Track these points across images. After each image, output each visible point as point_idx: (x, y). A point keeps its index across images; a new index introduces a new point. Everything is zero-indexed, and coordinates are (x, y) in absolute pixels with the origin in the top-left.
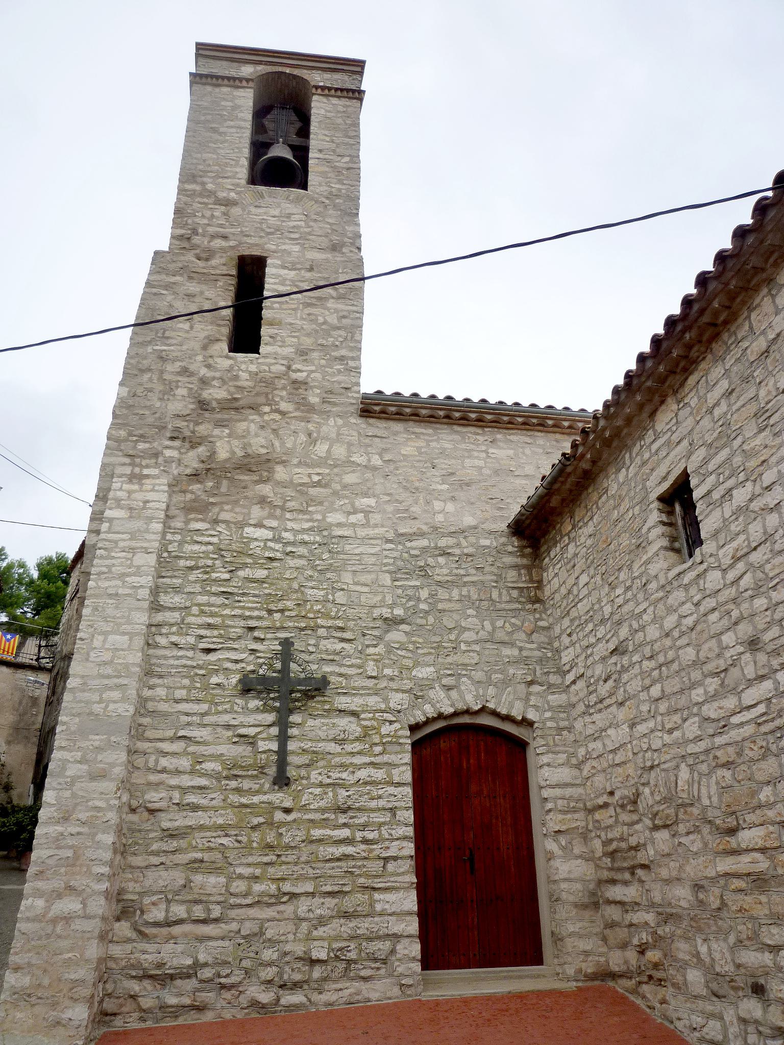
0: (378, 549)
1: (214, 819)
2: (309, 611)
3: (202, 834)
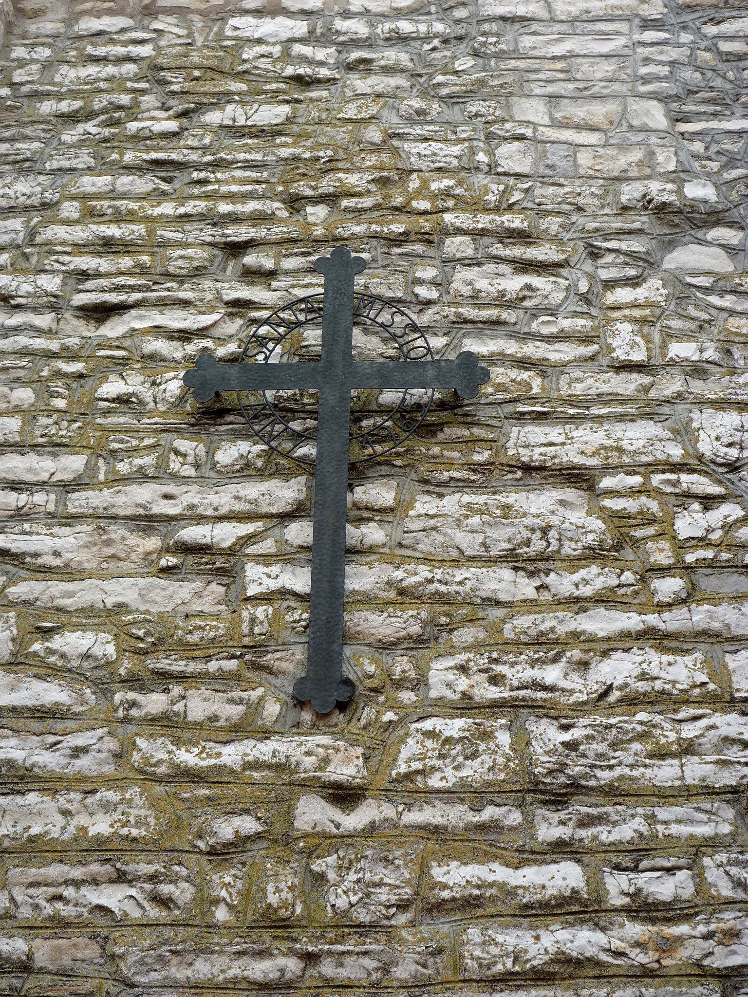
0: (621, 41)
1: (82, 820)
2: (417, 195)
3: (34, 873)
